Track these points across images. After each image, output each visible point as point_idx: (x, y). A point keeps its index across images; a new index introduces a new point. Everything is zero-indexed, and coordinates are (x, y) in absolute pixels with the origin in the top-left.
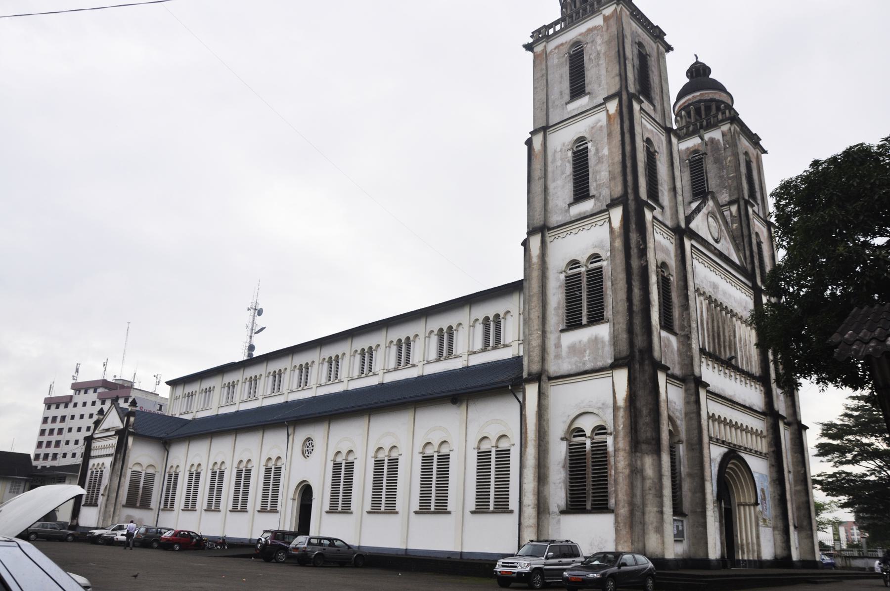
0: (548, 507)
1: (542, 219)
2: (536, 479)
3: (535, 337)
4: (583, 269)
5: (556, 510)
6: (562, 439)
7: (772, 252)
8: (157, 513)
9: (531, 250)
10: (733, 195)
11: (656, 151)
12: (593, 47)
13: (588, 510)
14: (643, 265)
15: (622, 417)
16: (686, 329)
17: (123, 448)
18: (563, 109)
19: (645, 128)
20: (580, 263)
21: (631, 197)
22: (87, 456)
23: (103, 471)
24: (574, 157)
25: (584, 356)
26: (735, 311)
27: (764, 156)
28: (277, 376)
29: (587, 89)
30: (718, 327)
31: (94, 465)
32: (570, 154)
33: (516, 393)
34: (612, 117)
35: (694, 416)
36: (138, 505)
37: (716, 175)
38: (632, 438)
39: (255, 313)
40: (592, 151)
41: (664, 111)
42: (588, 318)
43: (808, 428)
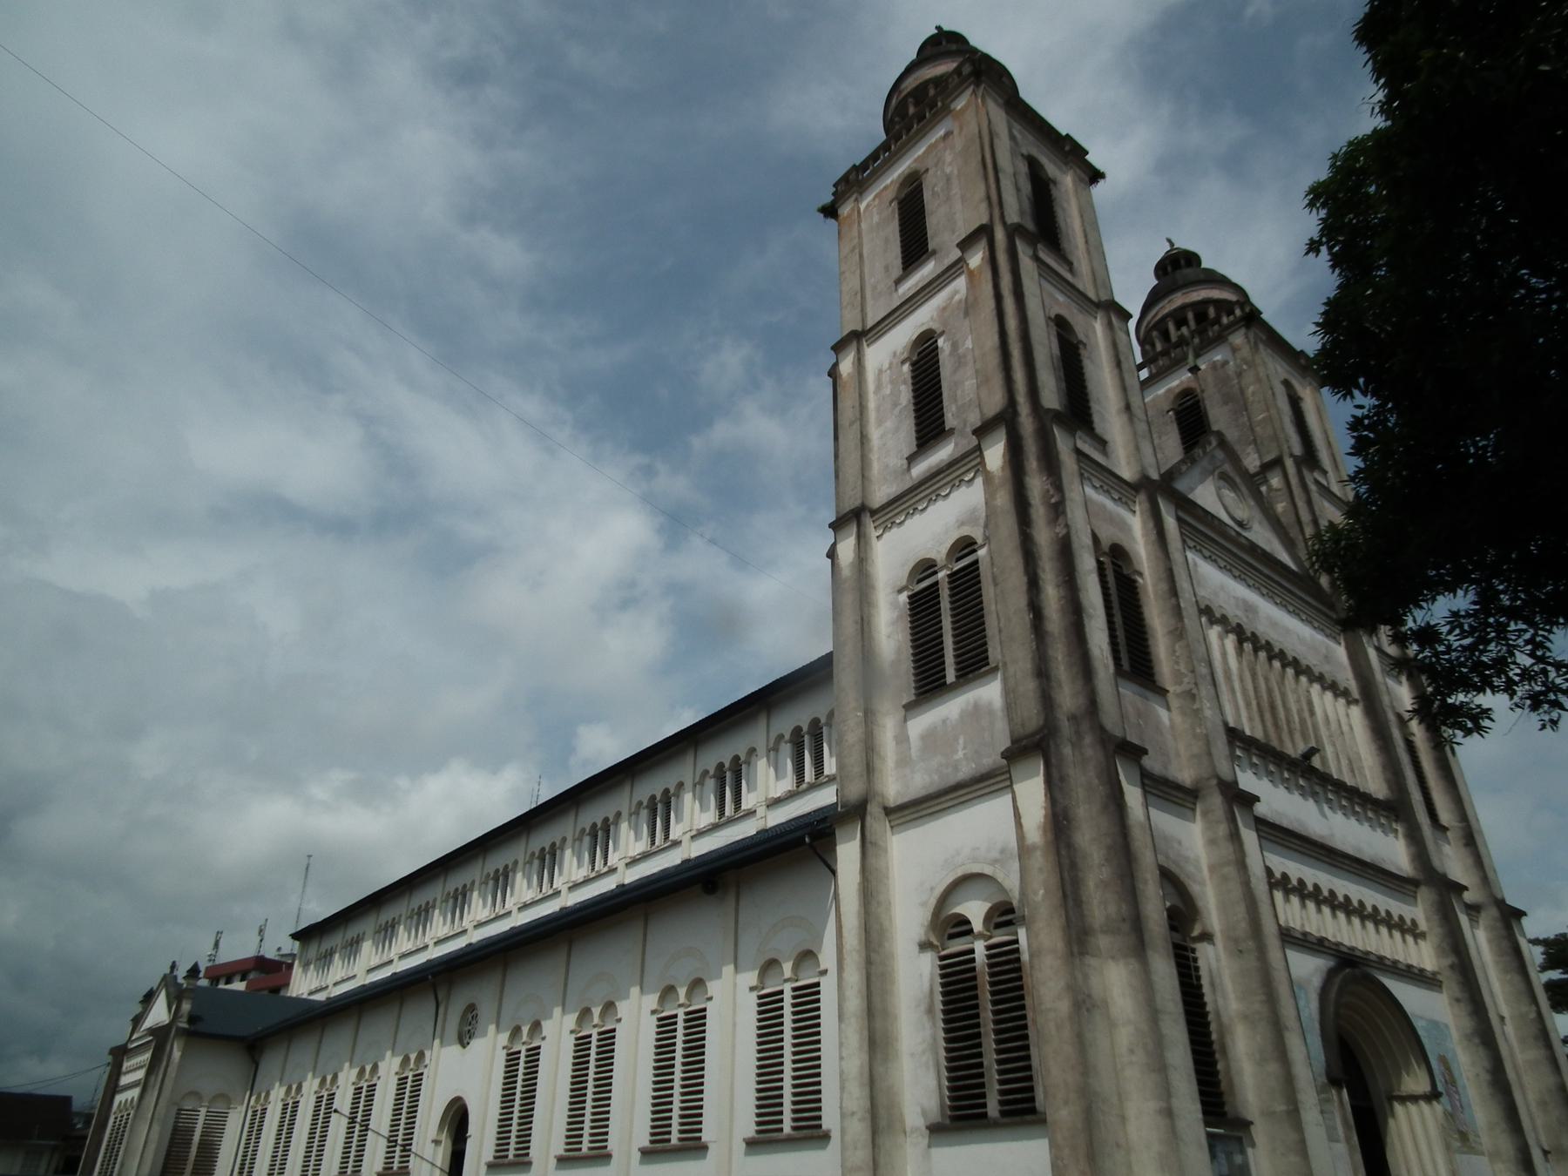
0: (902, 1115)
1: (859, 495)
2: (866, 1047)
4: (941, 575)
11: (1081, 342)
14: (1060, 535)
15: (1040, 870)
16: (1186, 680)
17: (164, 1063)
18: (891, 294)
24: (913, 371)
26: (1304, 662)
29: (931, 247)
30: (1270, 691)
31: (121, 1102)
32: (906, 368)
33: (827, 859)
35: (1231, 870)
40: (945, 348)
43: (1524, 914)
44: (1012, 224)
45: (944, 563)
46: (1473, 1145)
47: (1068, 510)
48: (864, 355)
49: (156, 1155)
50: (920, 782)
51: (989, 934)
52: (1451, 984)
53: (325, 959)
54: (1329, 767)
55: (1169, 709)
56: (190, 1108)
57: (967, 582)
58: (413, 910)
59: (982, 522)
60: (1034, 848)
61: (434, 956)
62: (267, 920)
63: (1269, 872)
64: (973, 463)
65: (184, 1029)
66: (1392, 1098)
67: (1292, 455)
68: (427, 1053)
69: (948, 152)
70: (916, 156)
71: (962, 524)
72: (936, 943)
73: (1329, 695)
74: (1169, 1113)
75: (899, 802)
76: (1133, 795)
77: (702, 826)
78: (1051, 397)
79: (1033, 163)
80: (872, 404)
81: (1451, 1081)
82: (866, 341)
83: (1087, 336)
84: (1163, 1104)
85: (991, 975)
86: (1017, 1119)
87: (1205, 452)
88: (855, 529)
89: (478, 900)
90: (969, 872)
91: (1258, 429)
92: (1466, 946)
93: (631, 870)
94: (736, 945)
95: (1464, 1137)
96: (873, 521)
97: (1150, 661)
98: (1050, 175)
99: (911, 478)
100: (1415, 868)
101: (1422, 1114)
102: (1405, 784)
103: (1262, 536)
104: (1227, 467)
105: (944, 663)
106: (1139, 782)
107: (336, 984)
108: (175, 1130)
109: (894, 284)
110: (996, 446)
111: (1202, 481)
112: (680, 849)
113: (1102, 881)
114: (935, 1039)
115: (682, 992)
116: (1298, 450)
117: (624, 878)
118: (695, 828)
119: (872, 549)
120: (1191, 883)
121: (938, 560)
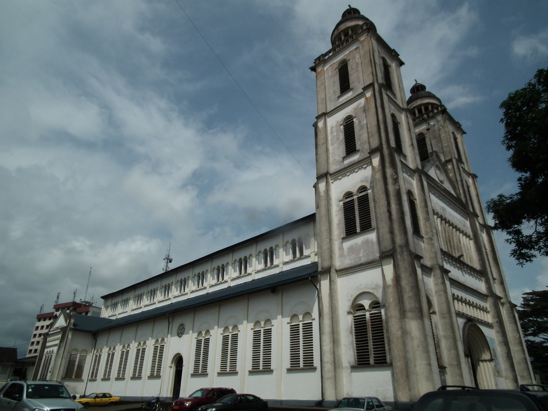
4: (355, 197)
7: (476, 192)
9: (320, 188)
11: (398, 122)
13: (371, 365)
14: (397, 189)
15: (392, 292)
16: (429, 234)
18: (336, 101)
19: (389, 109)
20: (352, 194)
21: (385, 146)
22: (44, 347)
23: (52, 355)
24: (344, 129)
25: (360, 254)
28: (167, 287)
29: (351, 87)
30: (449, 236)
31: (47, 351)
32: (342, 127)
34: (368, 99)
35: (442, 293)
39: (167, 261)
42: (360, 228)
44: (380, 83)
45: (356, 193)
46: (501, 375)
47: (399, 180)
48: (326, 121)
49: (64, 369)
50: (348, 262)
51: (370, 310)
52: (496, 327)
53: (115, 306)
54: (465, 260)
55: (424, 243)
56: (74, 354)
57: (364, 201)
58: (149, 291)
59: (369, 181)
60: (390, 286)
61: (158, 306)
62: (77, 289)
63: (453, 295)
64: (366, 162)
65: (72, 328)
66: (479, 360)
67: (455, 158)
68: (166, 339)
69: (357, 54)
70: (345, 54)
71: (362, 181)
72: (353, 312)
73: (464, 237)
74: (430, 365)
75: (341, 268)
76: (419, 271)
77: (259, 269)
78: (393, 144)
79: (384, 59)
80: (329, 138)
81: (495, 356)
82: (327, 116)
83: (400, 120)
84: (428, 362)
85: (371, 322)
86: (381, 365)
87: (432, 158)
88: (325, 180)
89: (174, 289)
90: (365, 291)
91: (445, 149)
92: (501, 316)
93: (232, 282)
94: (282, 309)
95: (498, 372)
96: (331, 177)
97: (419, 227)
98: (389, 64)
99: (344, 164)
100: (487, 292)
101: (487, 365)
102: (486, 266)
103: (447, 186)
104: (437, 163)
105: (356, 225)
106: (420, 267)
107: (119, 314)
108: (70, 361)
109: (337, 98)
110: (376, 158)
111: (431, 168)
112: (251, 276)
113: (409, 296)
114: (352, 340)
115: (262, 323)
116: (457, 157)
117: (230, 285)
118: (256, 269)
119: (330, 186)
120: (430, 297)
121: (354, 192)
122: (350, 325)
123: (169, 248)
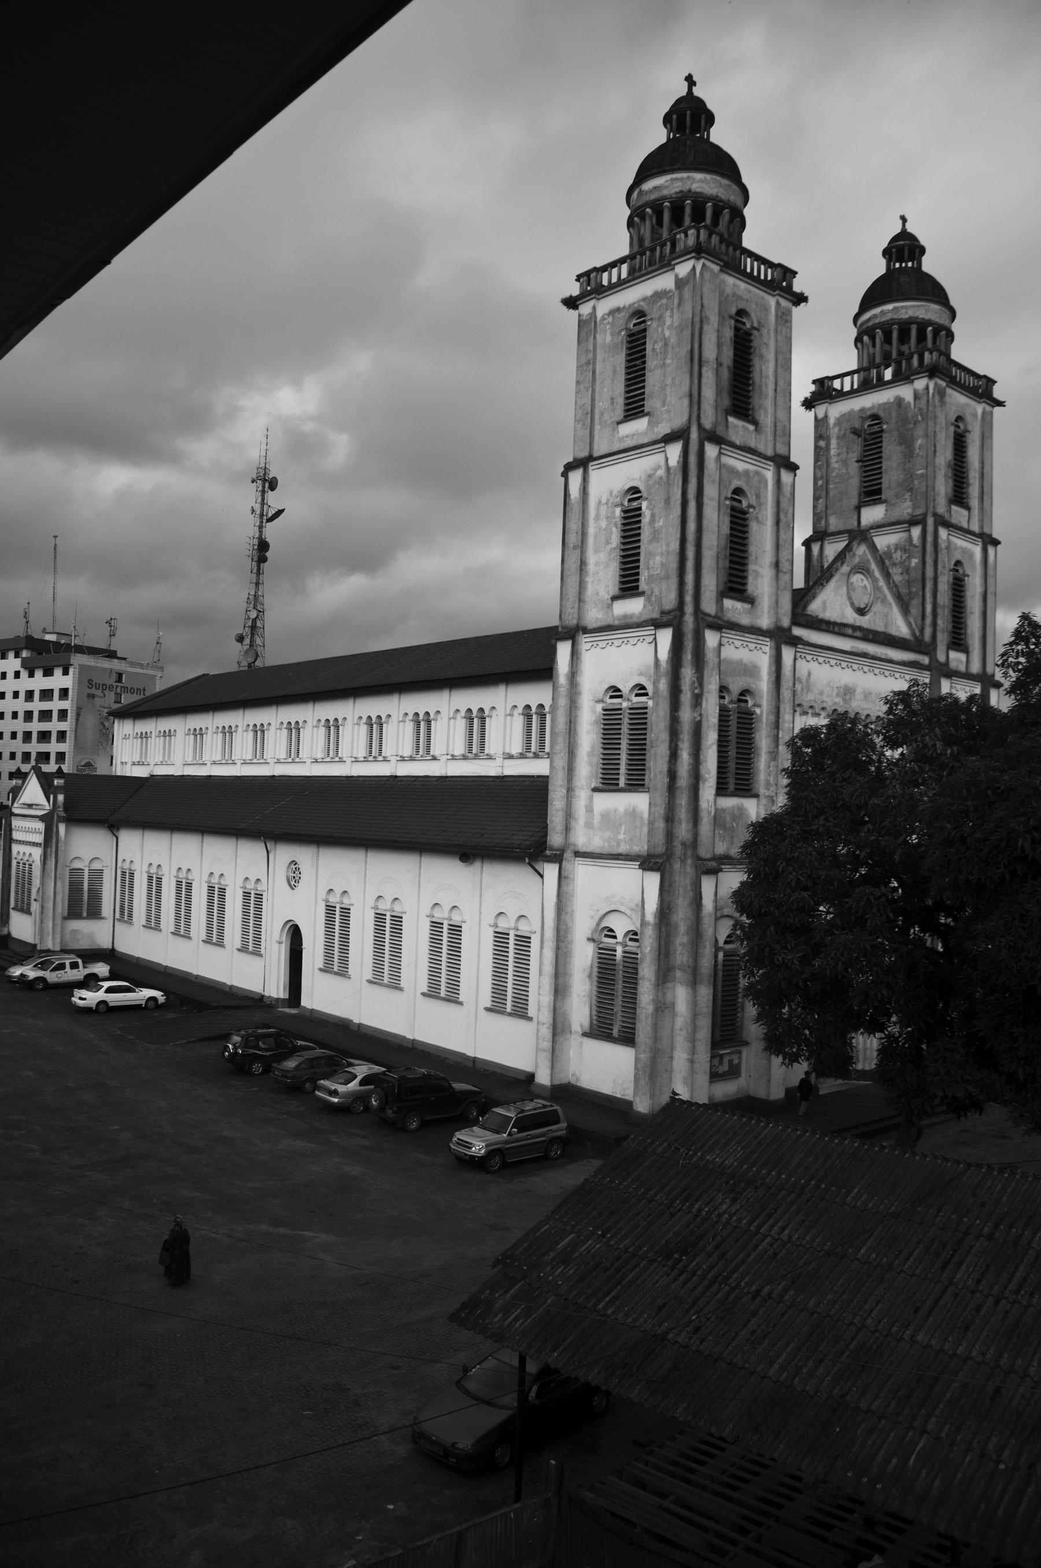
0: (570, 1024)
1: (576, 615)
2: (553, 992)
3: (559, 796)
5: (579, 1030)
6: (589, 939)
8: (112, 924)
10: (919, 507)
12: (660, 329)
16: (772, 789)
17: (54, 840)
21: (689, 609)
25: (619, 833)
27: (997, 410)
32: (618, 511)
36: (85, 914)
37: (899, 465)
38: (659, 965)
39: (264, 487)
41: (775, 426)
48: (588, 475)
60: (649, 924)
80: (591, 530)
114: (591, 992)
122: (589, 963)
123: (264, 447)
